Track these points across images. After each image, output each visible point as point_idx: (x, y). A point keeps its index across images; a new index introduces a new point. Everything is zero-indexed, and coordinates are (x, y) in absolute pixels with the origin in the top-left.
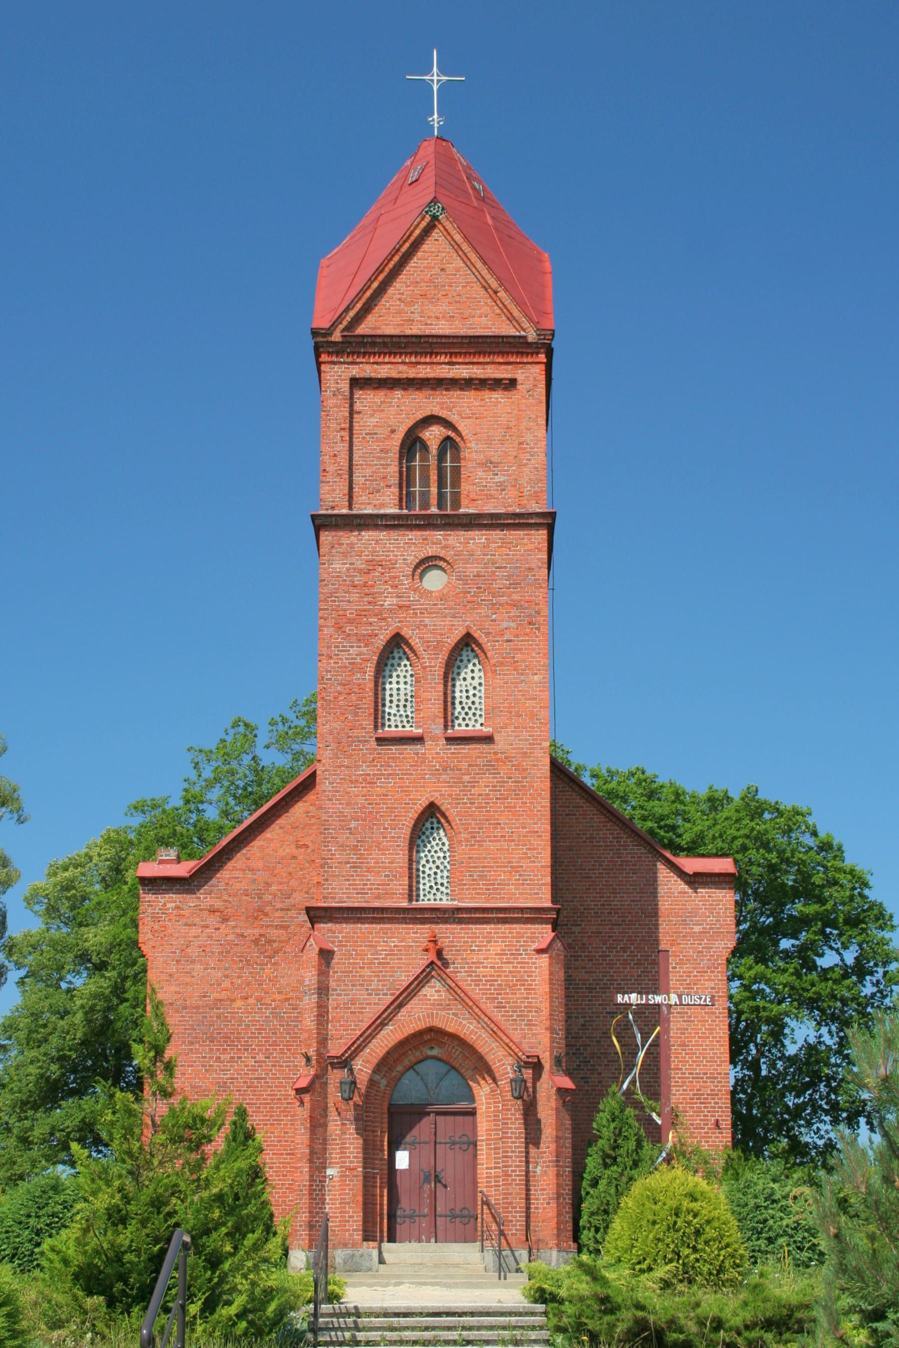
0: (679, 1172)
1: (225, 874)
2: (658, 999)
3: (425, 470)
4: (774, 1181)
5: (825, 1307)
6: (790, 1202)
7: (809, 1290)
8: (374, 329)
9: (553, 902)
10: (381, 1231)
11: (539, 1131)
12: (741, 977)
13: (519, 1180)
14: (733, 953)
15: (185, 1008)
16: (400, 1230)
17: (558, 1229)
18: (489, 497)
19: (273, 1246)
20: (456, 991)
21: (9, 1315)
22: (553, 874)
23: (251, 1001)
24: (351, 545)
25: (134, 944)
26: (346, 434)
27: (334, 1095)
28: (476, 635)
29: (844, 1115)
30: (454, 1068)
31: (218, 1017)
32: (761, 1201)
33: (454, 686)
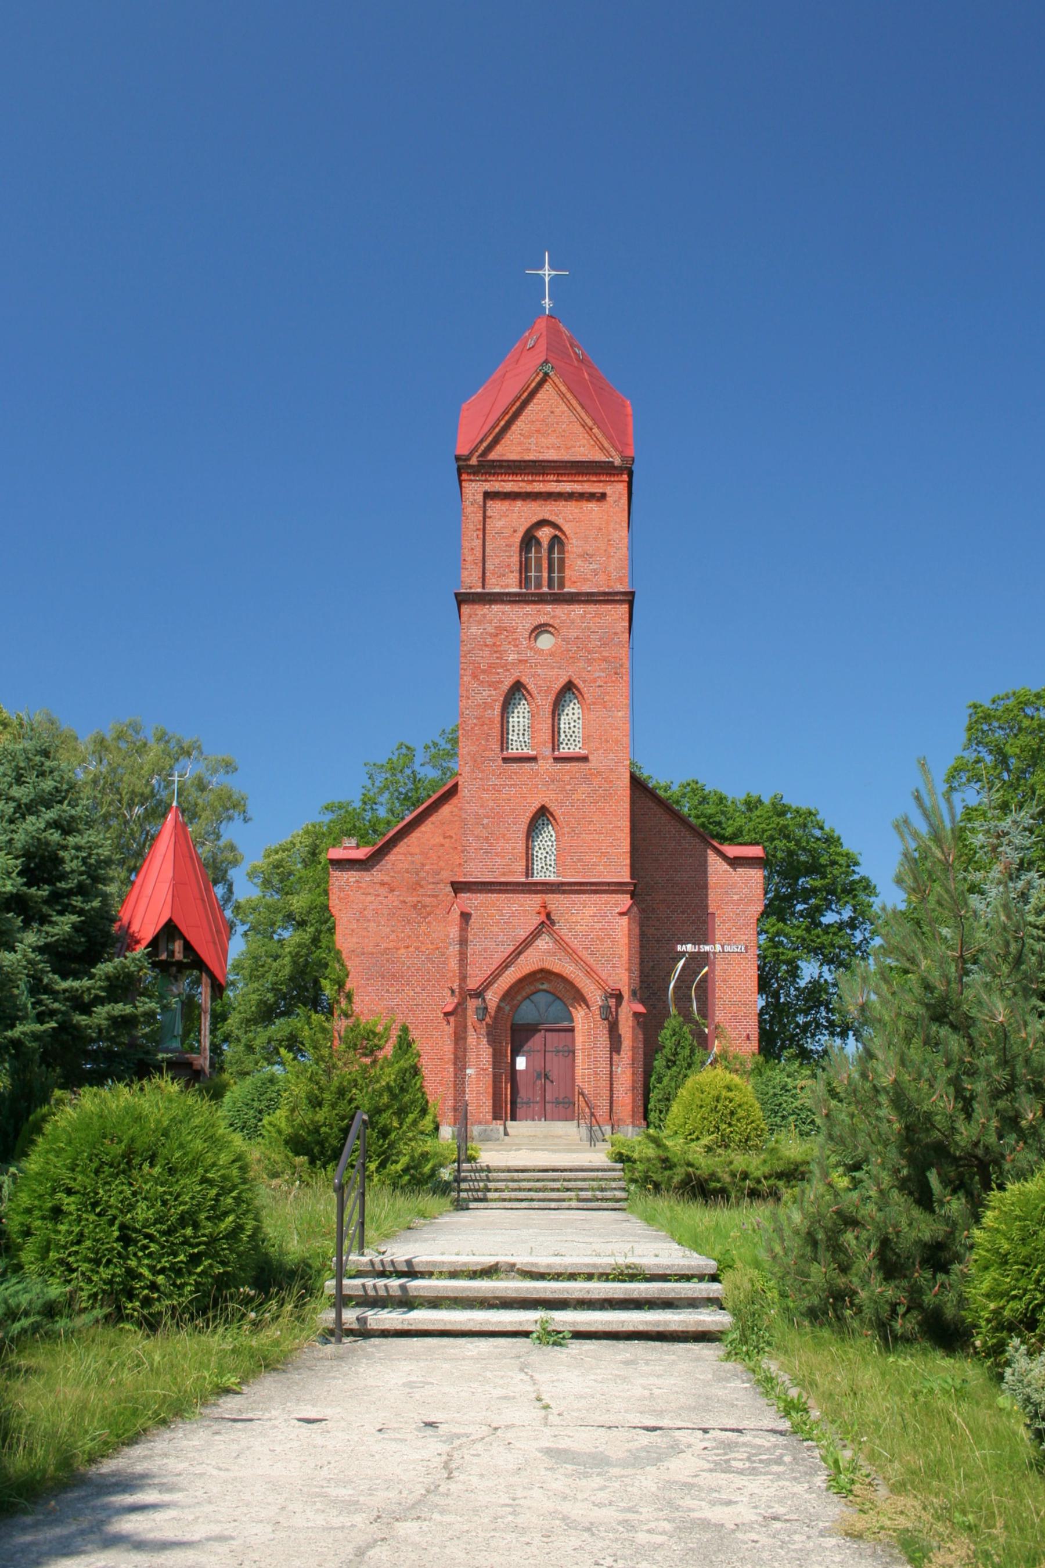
0: (719, 1070)
1: (391, 857)
2: (707, 948)
3: (538, 560)
4: (788, 1076)
5: (819, 1163)
6: (798, 1091)
7: (809, 1151)
8: (501, 455)
9: (632, 878)
10: (506, 1113)
11: (620, 1042)
12: (766, 932)
13: (605, 1077)
14: (762, 914)
15: (363, 954)
16: (519, 1112)
17: (633, 1111)
18: (586, 580)
19: (427, 1123)
20: (560, 943)
21: (240, 1168)
22: (632, 857)
23: (411, 949)
24: (484, 616)
25: (326, 908)
26: (481, 534)
27: (472, 1017)
28: (576, 682)
29: (839, 1030)
30: (558, 998)
31: (388, 961)
32: (778, 1091)
33: (559, 719)
